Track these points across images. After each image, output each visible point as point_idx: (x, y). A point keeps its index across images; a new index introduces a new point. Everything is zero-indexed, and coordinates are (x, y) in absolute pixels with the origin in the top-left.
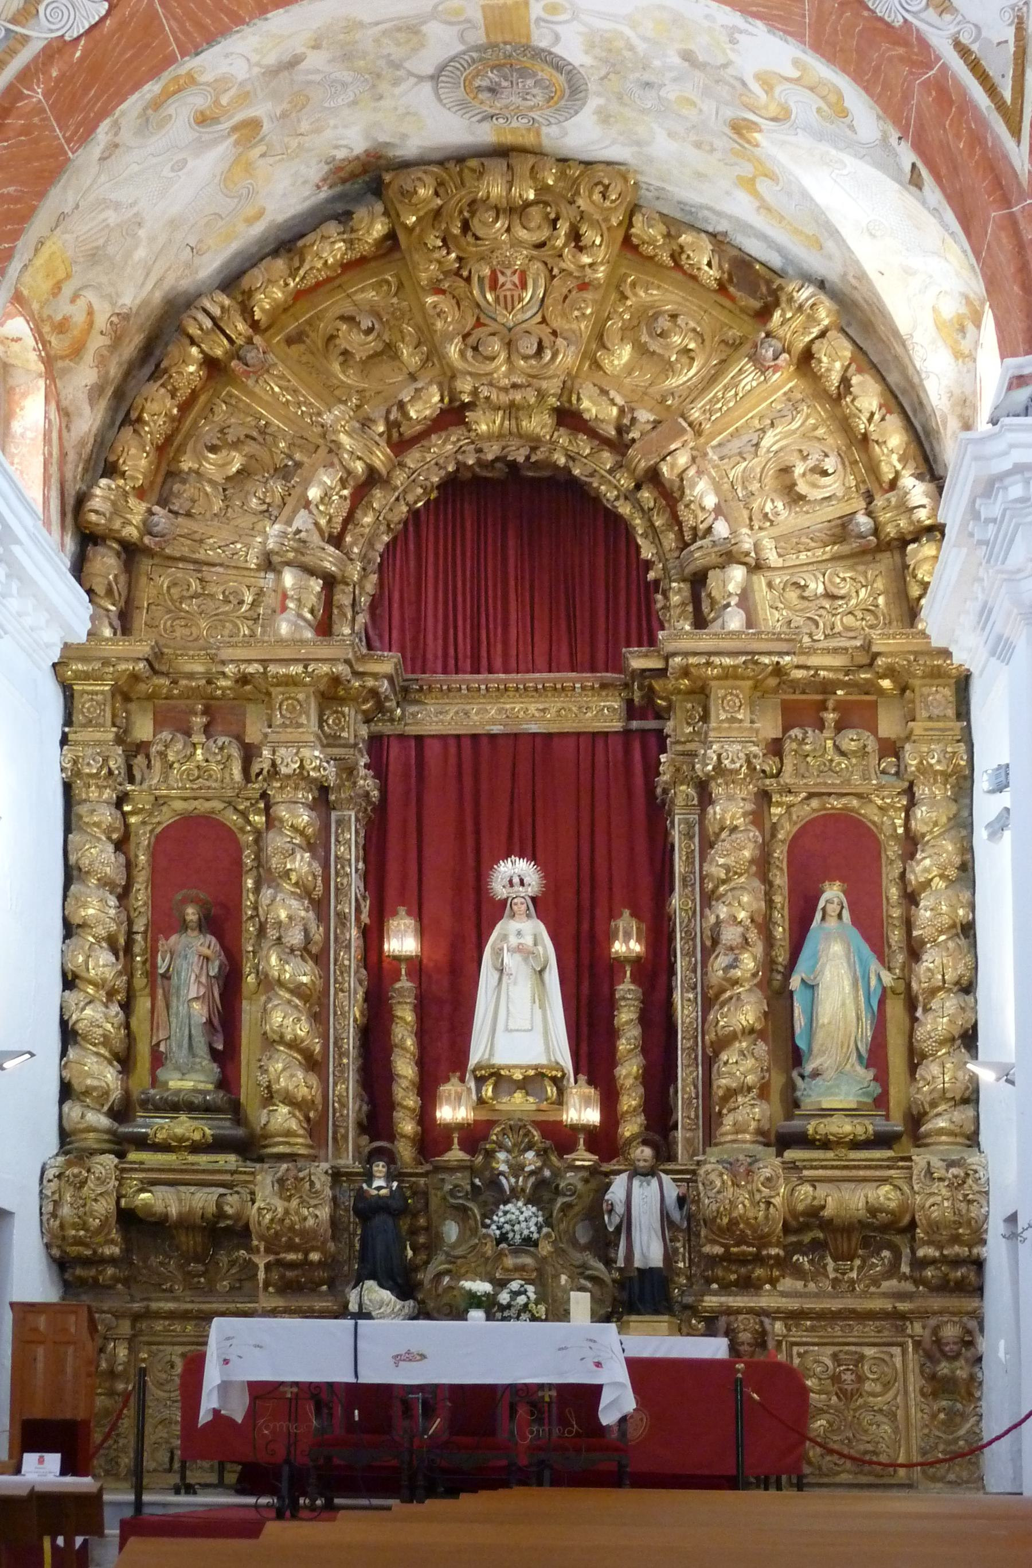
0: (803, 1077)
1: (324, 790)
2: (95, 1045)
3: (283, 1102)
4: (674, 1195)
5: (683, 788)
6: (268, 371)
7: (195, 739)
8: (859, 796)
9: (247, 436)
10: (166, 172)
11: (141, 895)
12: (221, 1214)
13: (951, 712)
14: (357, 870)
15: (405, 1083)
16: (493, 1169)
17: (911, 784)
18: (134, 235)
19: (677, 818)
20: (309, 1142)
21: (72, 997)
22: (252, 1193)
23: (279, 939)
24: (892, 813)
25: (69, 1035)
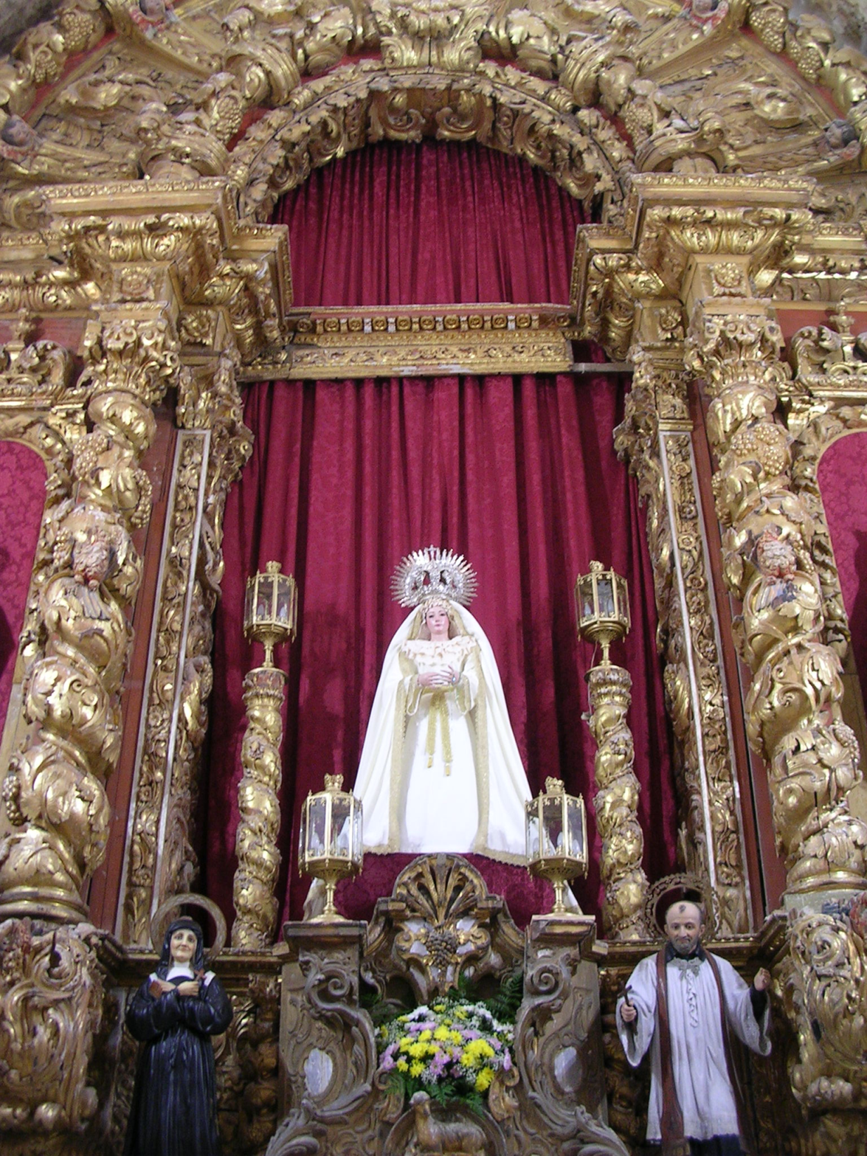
15: (255, 822)
16: (400, 949)
20: (76, 897)
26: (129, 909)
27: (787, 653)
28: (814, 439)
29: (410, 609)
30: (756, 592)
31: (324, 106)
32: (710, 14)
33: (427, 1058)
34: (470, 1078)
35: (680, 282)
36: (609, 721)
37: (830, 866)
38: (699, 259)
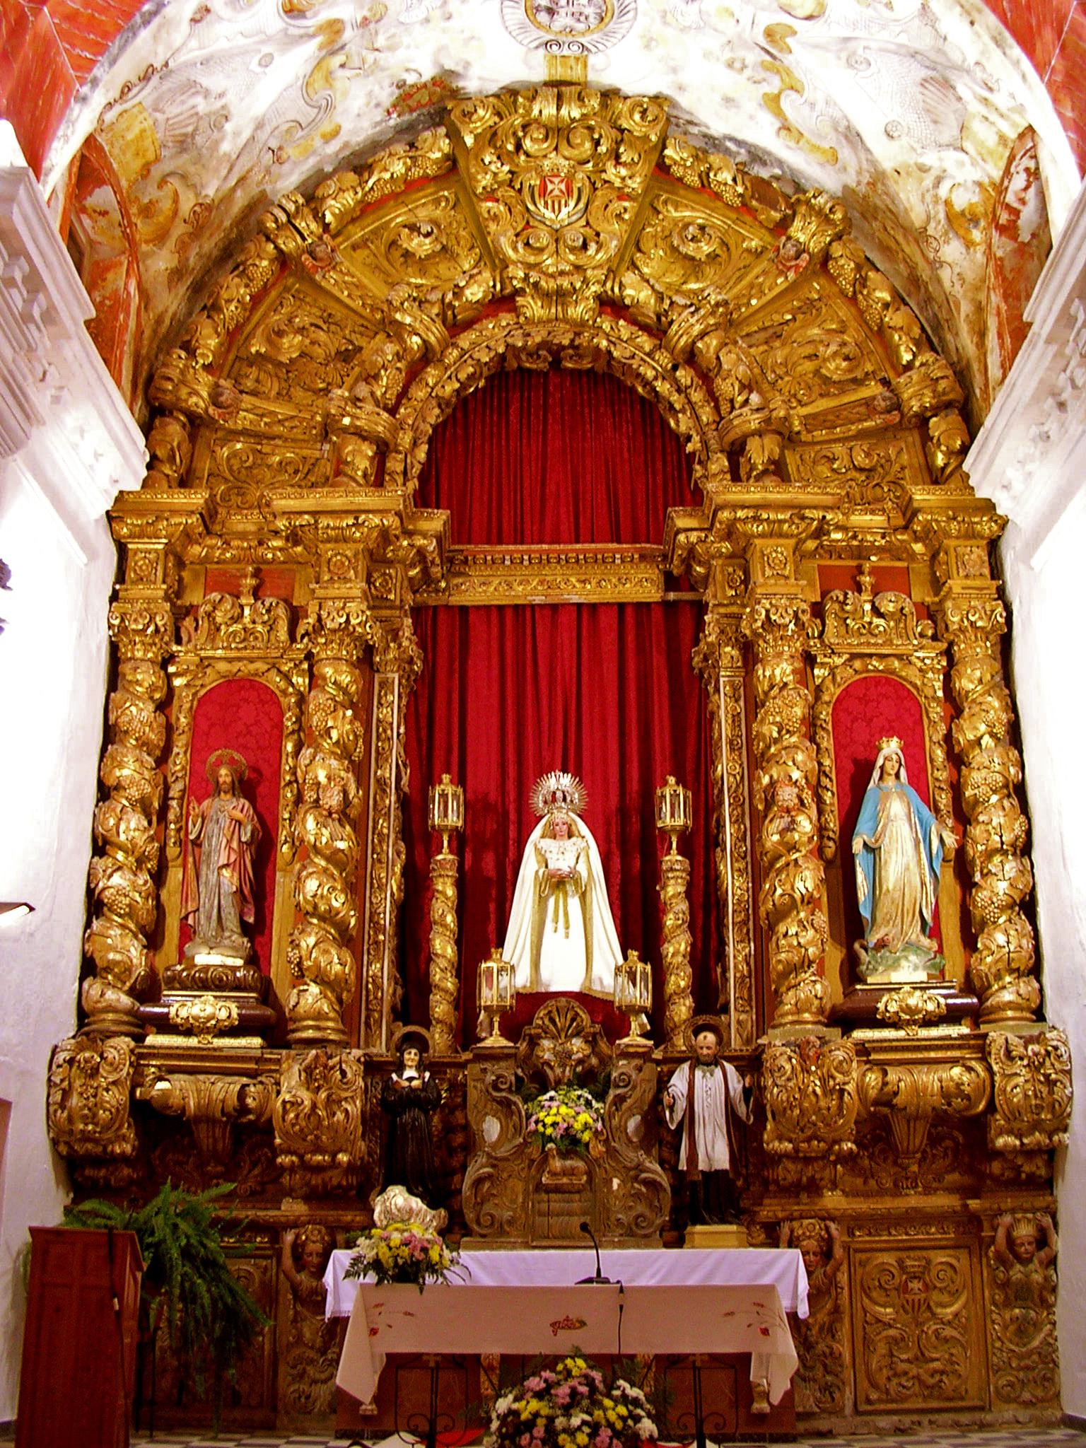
0: (866, 950)
1: (369, 650)
2: (120, 916)
3: (315, 982)
4: (739, 1087)
5: (728, 649)
6: (334, 268)
7: (243, 601)
8: (899, 657)
9: (312, 325)
10: (254, 66)
11: (180, 760)
12: (243, 1109)
13: (986, 571)
14: (399, 734)
15: (443, 963)
16: (538, 1057)
17: (951, 644)
18: (221, 128)
19: (722, 680)
20: (341, 1026)
21: (101, 863)
22: (278, 1084)
23: (317, 800)
24: (930, 675)
25: (95, 905)
26: (368, 1025)
27: (788, 864)
28: (831, 686)
29: (542, 817)
30: (771, 821)
31: (470, 361)
32: (793, 263)
33: (555, 1124)
34: (579, 1136)
35: (745, 550)
36: (673, 896)
37: (799, 1011)
38: (757, 541)
